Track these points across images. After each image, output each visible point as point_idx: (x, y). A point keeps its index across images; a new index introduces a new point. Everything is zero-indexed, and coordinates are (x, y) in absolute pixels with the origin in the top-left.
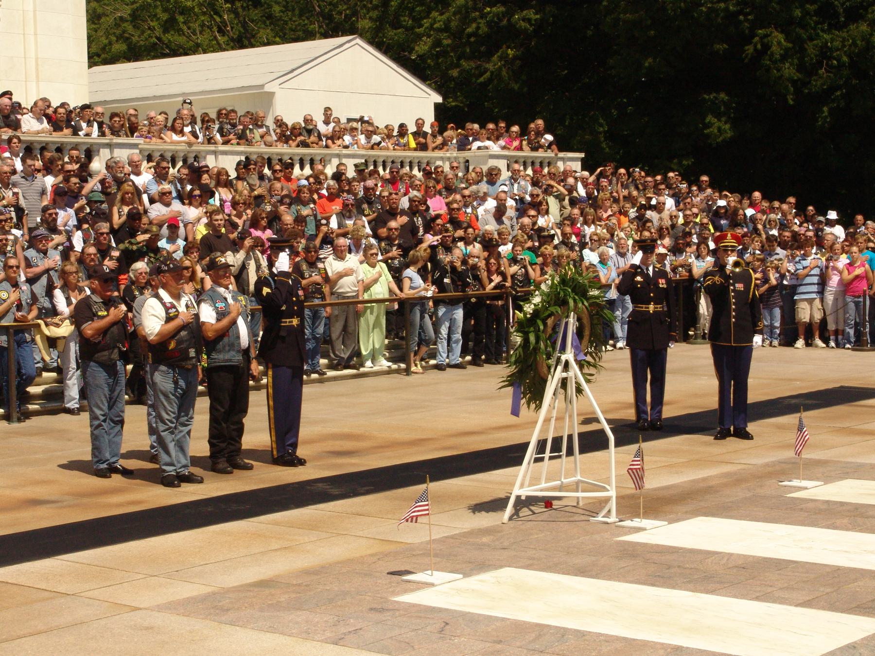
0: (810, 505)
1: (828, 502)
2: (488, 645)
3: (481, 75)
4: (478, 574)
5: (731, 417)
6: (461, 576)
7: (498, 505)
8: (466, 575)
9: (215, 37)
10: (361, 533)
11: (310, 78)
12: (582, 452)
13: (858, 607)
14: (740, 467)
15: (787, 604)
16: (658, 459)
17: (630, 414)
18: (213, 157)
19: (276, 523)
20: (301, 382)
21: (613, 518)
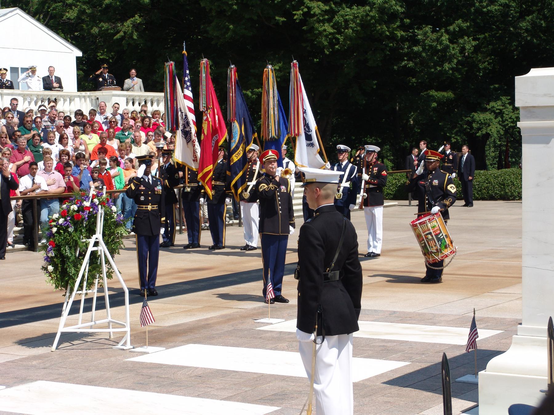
0: (268, 335)
1: (281, 332)
4: (18, 385)
5: (148, 289)
6: (5, 387)
7: (46, 339)
8: (8, 386)
12: (111, 306)
13: (261, 399)
14: (239, 310)
16: (183, 306)
19: (48, 323)
20: (349, 211)
21: (129, 346)
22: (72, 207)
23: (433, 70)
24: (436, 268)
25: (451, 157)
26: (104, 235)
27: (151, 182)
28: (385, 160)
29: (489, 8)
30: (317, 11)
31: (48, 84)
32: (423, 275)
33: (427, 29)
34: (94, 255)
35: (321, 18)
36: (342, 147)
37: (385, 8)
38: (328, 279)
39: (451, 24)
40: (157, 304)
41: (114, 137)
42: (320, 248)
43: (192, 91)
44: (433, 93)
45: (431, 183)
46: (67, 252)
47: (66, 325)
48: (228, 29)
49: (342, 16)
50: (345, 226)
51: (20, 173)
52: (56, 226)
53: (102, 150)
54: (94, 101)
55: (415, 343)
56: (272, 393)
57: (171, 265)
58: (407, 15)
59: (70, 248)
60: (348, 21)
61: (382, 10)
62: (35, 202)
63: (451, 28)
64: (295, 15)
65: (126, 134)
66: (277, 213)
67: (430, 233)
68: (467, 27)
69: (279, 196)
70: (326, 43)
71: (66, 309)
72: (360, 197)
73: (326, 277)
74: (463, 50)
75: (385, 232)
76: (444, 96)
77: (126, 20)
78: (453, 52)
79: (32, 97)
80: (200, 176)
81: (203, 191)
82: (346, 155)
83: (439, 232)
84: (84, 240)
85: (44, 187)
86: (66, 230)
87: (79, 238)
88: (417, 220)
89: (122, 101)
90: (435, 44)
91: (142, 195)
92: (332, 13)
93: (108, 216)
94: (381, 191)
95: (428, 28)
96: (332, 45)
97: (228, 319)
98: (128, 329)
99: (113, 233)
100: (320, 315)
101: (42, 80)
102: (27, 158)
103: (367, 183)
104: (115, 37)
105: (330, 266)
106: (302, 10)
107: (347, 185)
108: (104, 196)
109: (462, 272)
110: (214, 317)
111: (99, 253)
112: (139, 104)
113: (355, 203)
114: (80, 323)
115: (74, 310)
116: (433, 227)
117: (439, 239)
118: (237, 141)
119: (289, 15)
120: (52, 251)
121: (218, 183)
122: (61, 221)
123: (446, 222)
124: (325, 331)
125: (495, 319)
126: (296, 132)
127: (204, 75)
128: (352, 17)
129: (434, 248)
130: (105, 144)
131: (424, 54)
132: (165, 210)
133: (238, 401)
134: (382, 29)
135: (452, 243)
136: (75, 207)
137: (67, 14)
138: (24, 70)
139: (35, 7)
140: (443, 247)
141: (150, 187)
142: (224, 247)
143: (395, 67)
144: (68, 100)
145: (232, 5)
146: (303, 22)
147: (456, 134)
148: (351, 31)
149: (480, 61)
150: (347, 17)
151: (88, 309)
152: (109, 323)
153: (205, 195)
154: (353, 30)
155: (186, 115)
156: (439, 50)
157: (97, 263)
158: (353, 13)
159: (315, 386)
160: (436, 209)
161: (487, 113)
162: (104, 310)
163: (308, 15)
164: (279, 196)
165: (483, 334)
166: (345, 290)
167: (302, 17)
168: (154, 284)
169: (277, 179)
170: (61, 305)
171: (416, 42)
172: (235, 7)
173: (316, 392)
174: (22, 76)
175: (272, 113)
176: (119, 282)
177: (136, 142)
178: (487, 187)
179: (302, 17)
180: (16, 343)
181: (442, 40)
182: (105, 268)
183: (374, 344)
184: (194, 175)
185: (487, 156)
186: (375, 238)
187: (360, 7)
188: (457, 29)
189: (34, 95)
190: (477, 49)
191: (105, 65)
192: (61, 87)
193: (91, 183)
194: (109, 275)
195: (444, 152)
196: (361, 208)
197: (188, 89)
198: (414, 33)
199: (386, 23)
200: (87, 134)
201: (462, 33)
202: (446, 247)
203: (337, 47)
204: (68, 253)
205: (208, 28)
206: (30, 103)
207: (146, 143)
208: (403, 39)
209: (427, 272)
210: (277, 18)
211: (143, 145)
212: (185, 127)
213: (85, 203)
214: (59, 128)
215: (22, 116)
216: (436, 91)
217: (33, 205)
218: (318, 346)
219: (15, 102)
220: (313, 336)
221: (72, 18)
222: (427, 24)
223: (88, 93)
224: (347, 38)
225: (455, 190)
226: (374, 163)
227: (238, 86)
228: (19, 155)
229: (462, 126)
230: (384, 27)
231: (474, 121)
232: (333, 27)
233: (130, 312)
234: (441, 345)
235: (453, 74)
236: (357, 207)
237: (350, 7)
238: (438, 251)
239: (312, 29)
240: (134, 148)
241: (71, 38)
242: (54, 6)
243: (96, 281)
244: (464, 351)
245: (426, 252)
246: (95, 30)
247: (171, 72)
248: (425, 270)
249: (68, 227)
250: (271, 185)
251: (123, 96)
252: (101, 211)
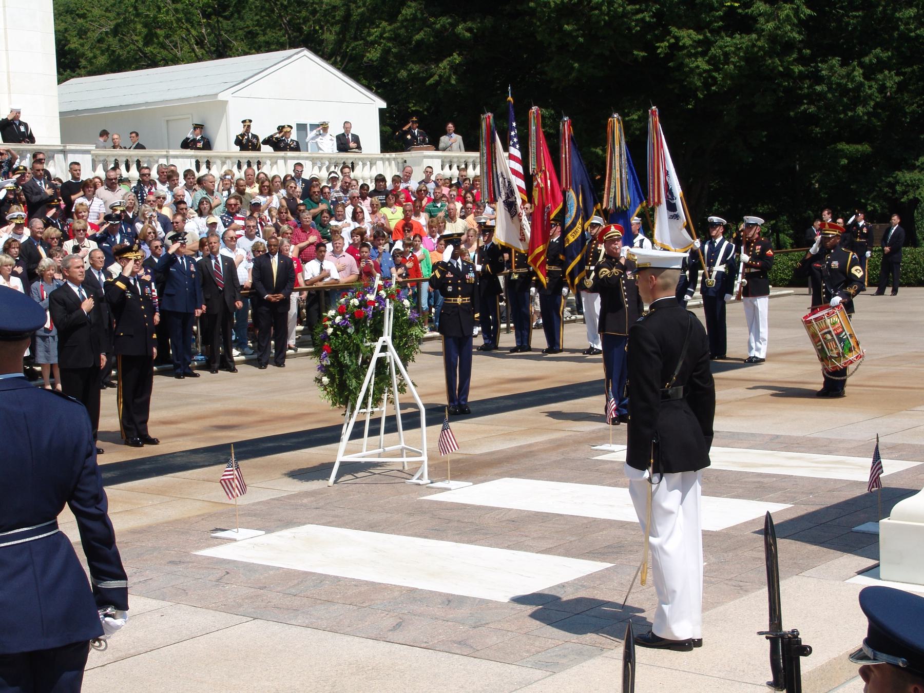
2: (253, 590)
3: (428, 79)
5: (458, 406)
7: (321, 471)
8: (268, 531)
9: (193, 50)
10: (200, 497)
11: (263, 87)
14: (570, 433)
15: (530, 551)
16: (501, 428)
17: (443, 400)
18: (283, 161)
19: (132, 490)
20: (724, 303)
21: (426, 480)
22: (352, 302)
23: (842, 116)
25: (865, 231)
26: (394, 338)
27: (460, 267)
28: (782, 236)
29: (918, 32)
30: (688, 42)
31: (343, 144)
32: (819, 387)
33: (834, 62)
34: (382, 364)
35: (693, 51)
36: (715, 219)
37: (778, 35)
38: (669, 397)
39: (866, 55)
40: (468, 425)
41: (423, 210)
42: (655, 356)
43: (520, 149)
44: (843, 146)
45: (829, 265)
46: (346, 359)
47: (347, 452)
48: (573, 68)
49: (721, 48)
50: (691, 327)
51: (304, 257)
52: (332, 326)
53: (407, 225)
54: (401, 165)
55: (802, 478)
56: (605, 544)
57: (488, 374)
58: (806, 43)
59: (350, 354)
60: (729, 54)
61: (773, 39)
62: (323, 294)
63: (867, 60)
64: (659, 47)
65: (439, 205)
66: (622, 306)
67: (830, 332)
68: (888, 57)
69: (624, 285)
70: (699, 84)
71: (347, 432)
72: (739, 281)
73: (665, 396)
74: (882, 89)
75: (769, 328)
76: (857, 150)
77: (442, 61)
78: (869, 92)
79: (323, 161)
80: (529, 259)
81: (534, 278)
82: (721, 230)
83: (841, 330)
84: (368, 344)
85: (335, 275)
86: (344, 332)
87: (362, 342)
88: (810, 315)
89: (436, 165)
90: (844, 81)
91: (450, 285)
92: (706, 44)
93: (399, 312)
94: (766, 277)
95: (835, 61)
96: (706, 85)
97: (558, 445)
98: (424, 458)
99: (406, 334)
100: (656, 446)
101: (335, 139)
102: (313, 239)
103: (746, 265)
104: (428, 83)
105: (670, 380)
106: (668, 41)
107: (722, 268)
108: (393, 286)
109: (872, 383)
110: (540, 443)
111: (388, 361)
112: (458, 167)
113: (731, 293)
114: (365, 450)
115: (357, 433)
116: (834, 324)
117: (841, 340)
118: (573, 216)
119: (650, 48)
120: (327, 358)
121: (553, 268)
122: (338, 319)
123: (850, 316)
124: (664, 468)
125: (913, 446)
126: (656, 200)
127: (533, 128)
128: (733, 49)
129: (835, 351)
130: (410, 218)
131: (830, 96)
132: (480, 304)
133: (559, 555)
134: (773, 63)
135: (858, 344)
136: (356, 302)
137: (368, 55)
138: (313, 127)
139: (330, 47)
141: (460, 275)
142: (561, 351)
143: (792, 114)
144: (368, 163)
145: (578, 36)
146: (670, 56)
147: (874, 200)
148: (732, 67)
149: (906, 102)
150: (727, 49)
151: (374, 432)
152: (402, 450)
153: (538, 285)
154: (735, 66)
155: (509, 182)
156: (850, 90)
157: (385, 373)
158: (736, 44)
159: (651, 539)
160: (837, 300)
161: (916, 171)
162: (395, 434)
163: (675, 47)
164: (624, 285)
165: (891, 467)
166: (692, 413)
167: (667, 50)
168: (466, 399)
169: (622, 261)
170: (341, 426)
171: (819, 80)
172: (581, 40)
173: (652, 547)
174: (311, 134)
175: (618, 176)
176: (413, 397)
177: (450, 217)
178: (915, 269)
179: (667, 50)
180: (285, 474)
181: (854, 77)
182: (395, 380)
183: (747, 480)
184: (522, 260)
185: (918, 228)
186: (757, 338)
187: (744, 35)
188: (875, 61)
189: (325, 158)
190: (901, 87)
191: (414, 119)
192: (359, 147)
193: (393, 269)
194: (402, 388)
195: (855, 223)
196: (738, 298)
197: (515, 147)
198: (816, 67)
199: (778, 55)
200: (390, 207)
201: (882, 65)
202: (850, 350)
203: (713, 88)
204: (347, 361)
205: (546, 68)
206: (320, 168)
207: (463, 217)
208: (802, 76)
209: (825, 383)
210: (635, 52)
211: (459, 220)
212: (508, 197)
213: (368, 296)
214: (352, 199)
215: (310, 184)
216: (848, 143)
217: (321, 297)
218: (654, 487)
219: (299, 169)
220: (647, 474)
221: (375, 59)
222: (834, 56)
223: (394, 155)
224: (727, 76)
225: (862, 273)
226: (757, 239)
227: (574, 144)
228: (302, 235)
229: (880, 190)
230: (777, 61)
231: (897, 182)
232: (708, 62)
233: (426, 435)
234: (836, 480)
235: (869, 120)
236: (733, 298)
237: (731, 36)
238: (840, 356)
239: (682, 65)
240: (448, 224)
241: (378, 87)
242: (353, 45)
243: (385, 396)
244: (866, 491)
245: (823, 357)
246: (403, 74)
247: (489, 127)
248: (823, 380)
249: (347, 327)
250: (614, 270)
251: (438, 157)
252: (389, 306)
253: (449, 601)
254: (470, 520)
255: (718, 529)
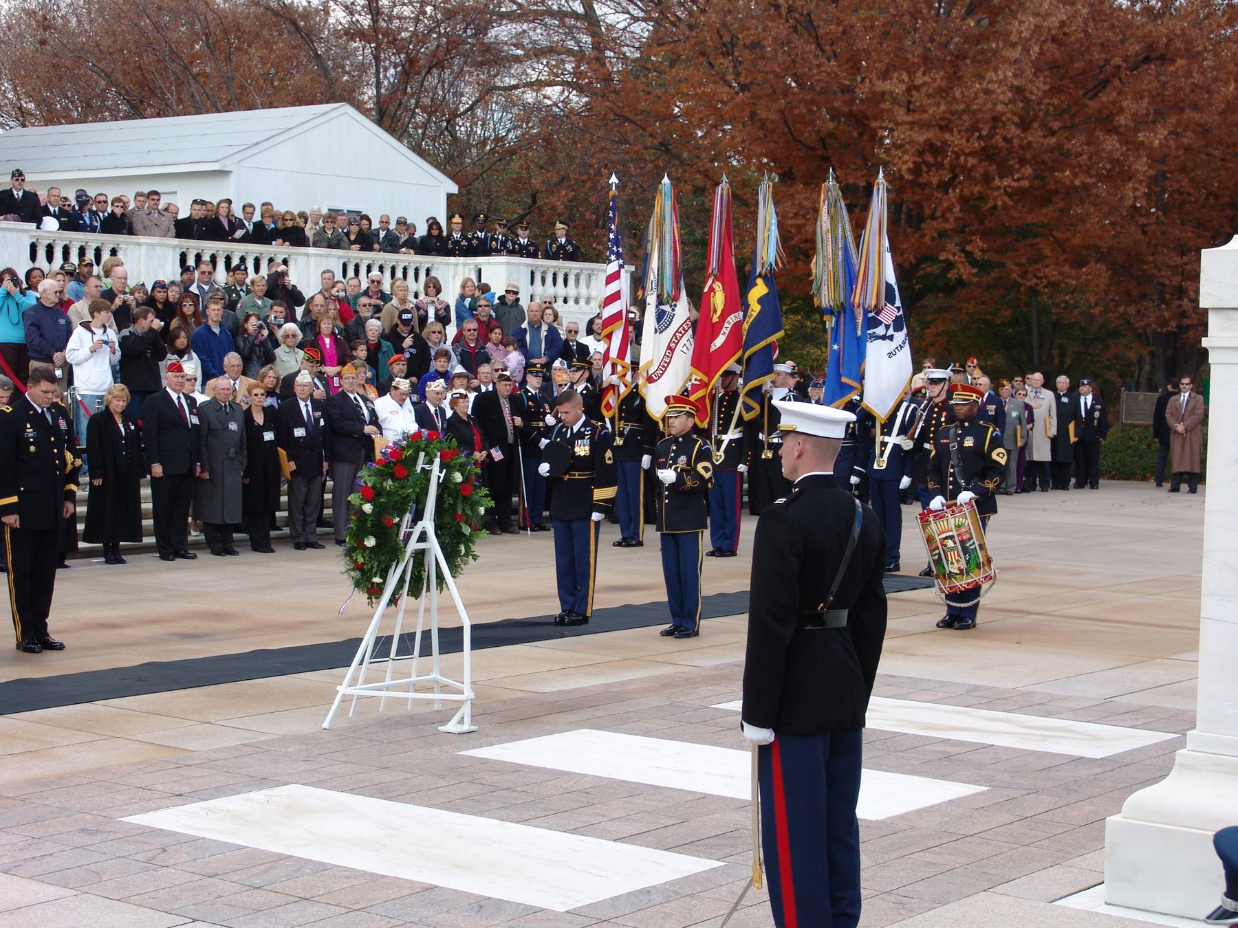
10: (140, 737)
16: (585, 656)
19: (42, 721)
24: (962, 605)
40: (538, 650)
97: (664, 685)
98: (468, 694)
140: (973, 566)
151: (426, 651)
223: (462, 260)
253: (481, 907)
254: (525, 789)
255: (879, 818)
